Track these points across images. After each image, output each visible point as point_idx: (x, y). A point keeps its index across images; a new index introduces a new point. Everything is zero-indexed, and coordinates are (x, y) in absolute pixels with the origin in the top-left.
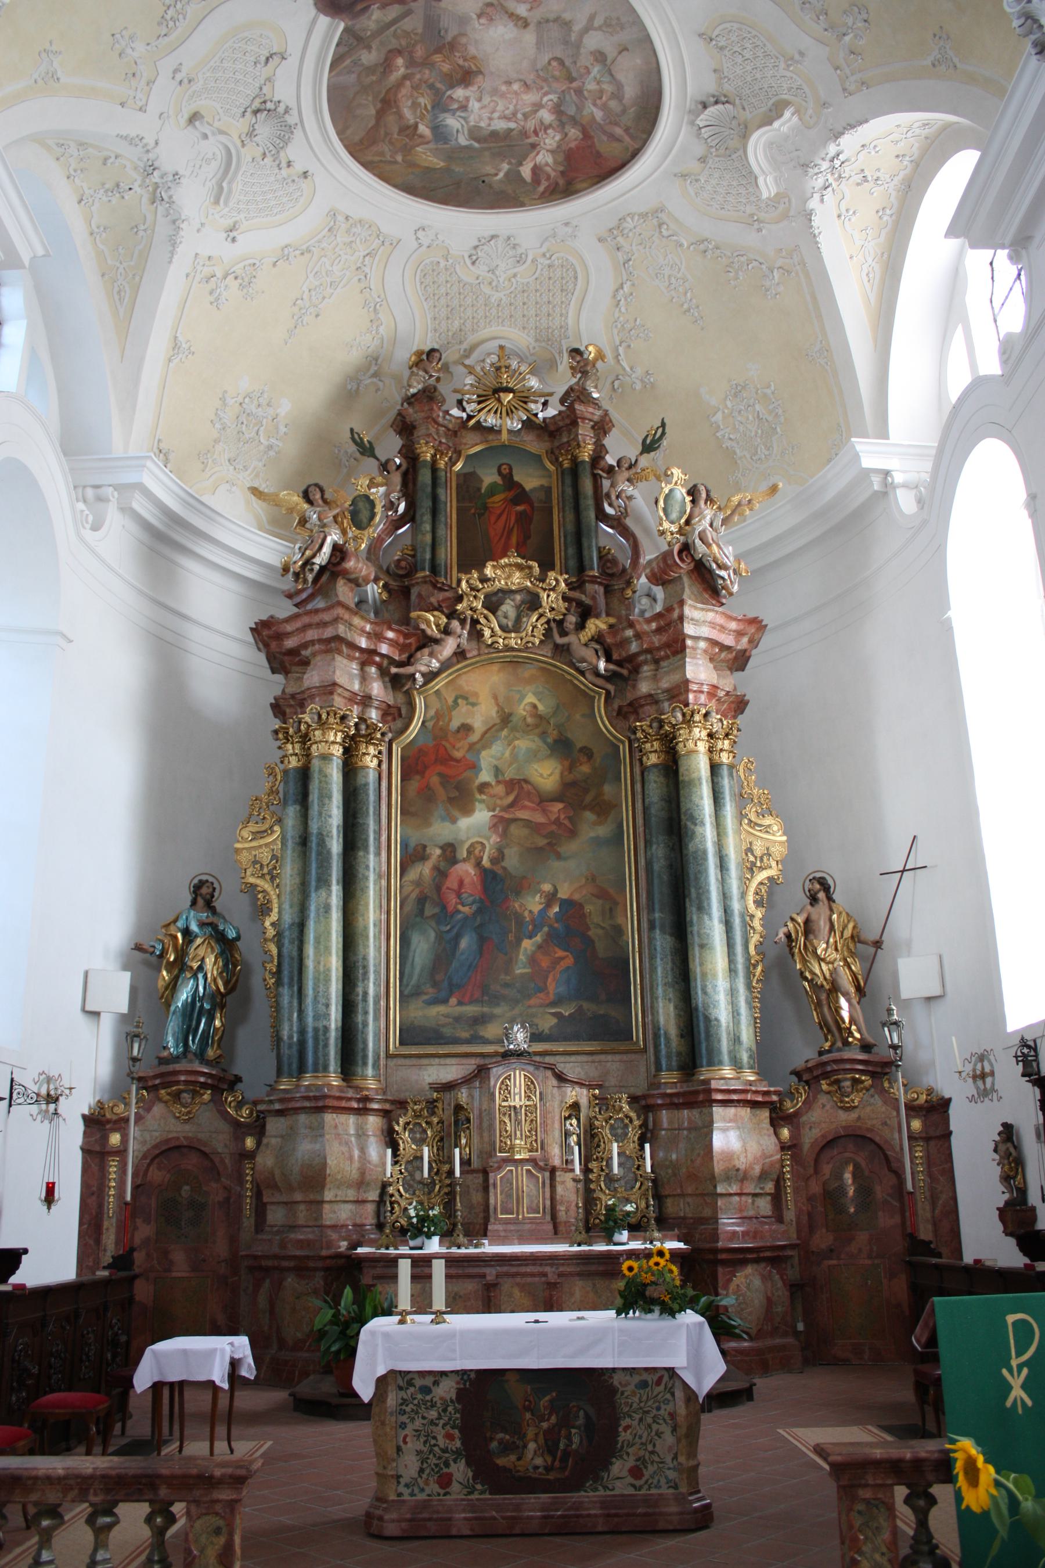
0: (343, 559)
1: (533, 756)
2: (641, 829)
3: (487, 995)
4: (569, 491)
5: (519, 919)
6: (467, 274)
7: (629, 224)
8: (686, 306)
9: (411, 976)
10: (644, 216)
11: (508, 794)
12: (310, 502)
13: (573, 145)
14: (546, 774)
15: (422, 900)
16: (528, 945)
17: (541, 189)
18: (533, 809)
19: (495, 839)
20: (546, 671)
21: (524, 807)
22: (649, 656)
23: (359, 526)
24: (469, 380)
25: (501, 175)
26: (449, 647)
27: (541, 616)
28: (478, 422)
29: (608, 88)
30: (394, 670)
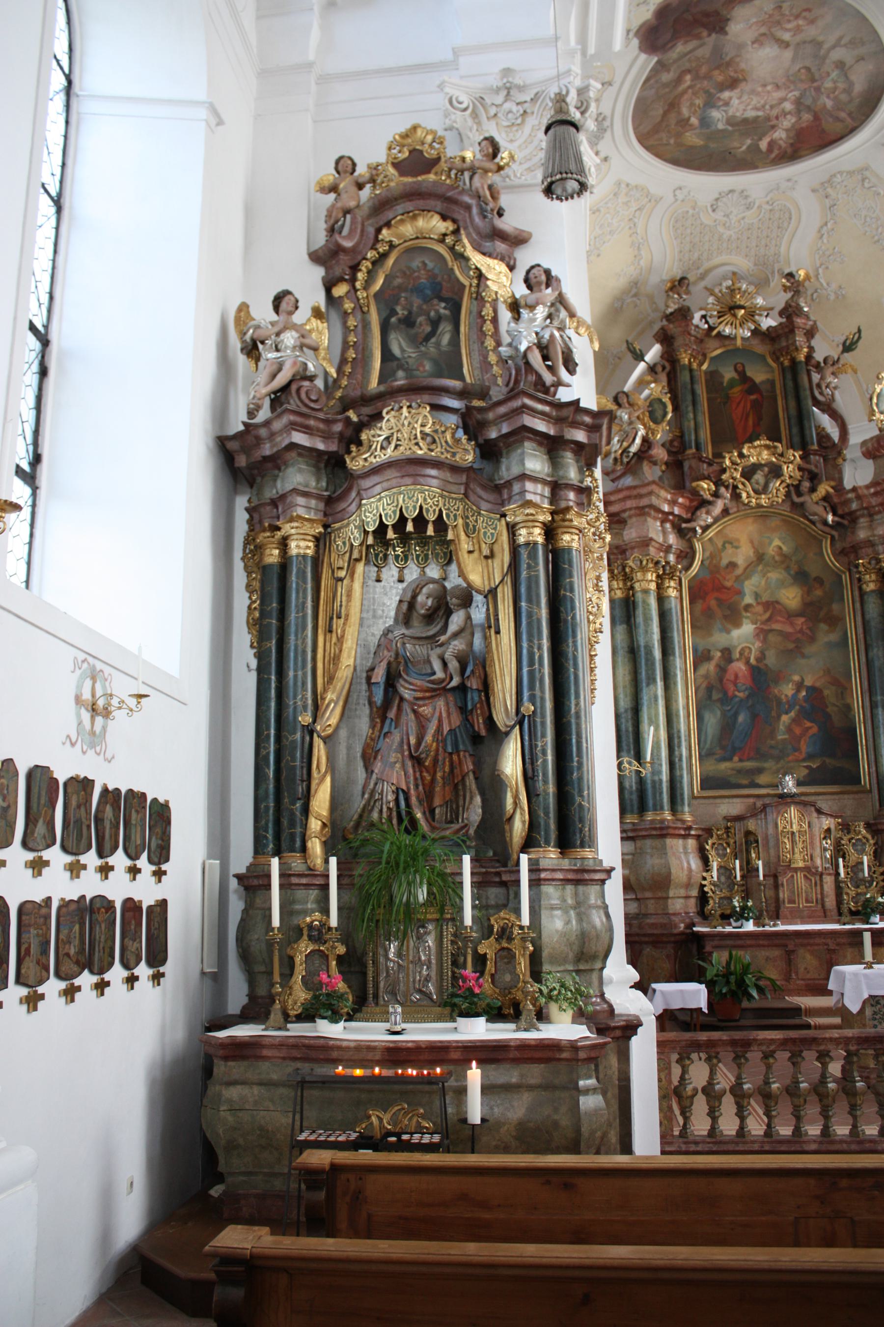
0: (650, 447)
1: (782, 584)
2: (861, 636)
3: (761, 756)
4: (790, 384)
5: (779, 702)
6: (707, 219)
7: (839, 178)
8: (876, 238)
9: (705, 742)
10: (851, 173)
11: (765, 612)
12: (619, 405)
13: (804, 125)
14: (791, 597)
15: (710, 689)
16: (785, 719)
17: (773, 156)
18: (784, 623)
19: (758, 644)
20: (786, 522)
21: (777, 621)
22: (866, 512)
23: (656, 422)
24: (711, 300)
25: (744, 148)
26: (718, 509)
27: (782, 482)
28: (719, 333)
29: (841, 85)
30: (684, 525)
